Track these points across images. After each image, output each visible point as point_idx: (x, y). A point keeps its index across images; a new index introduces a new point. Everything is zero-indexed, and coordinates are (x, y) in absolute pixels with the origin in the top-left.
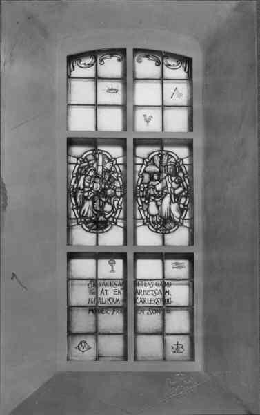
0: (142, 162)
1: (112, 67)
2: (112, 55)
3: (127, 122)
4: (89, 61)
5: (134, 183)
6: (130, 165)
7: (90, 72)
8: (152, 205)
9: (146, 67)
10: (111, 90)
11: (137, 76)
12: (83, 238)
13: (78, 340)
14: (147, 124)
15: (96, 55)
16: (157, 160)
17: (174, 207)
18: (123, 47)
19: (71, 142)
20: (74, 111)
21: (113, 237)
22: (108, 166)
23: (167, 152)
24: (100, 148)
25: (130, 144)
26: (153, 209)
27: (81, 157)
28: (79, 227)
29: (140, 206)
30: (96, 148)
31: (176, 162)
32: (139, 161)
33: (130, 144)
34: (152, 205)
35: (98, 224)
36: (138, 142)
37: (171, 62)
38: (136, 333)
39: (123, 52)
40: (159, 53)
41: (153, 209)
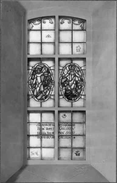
0: (62, 69)
1: (48, 24)
3: (57, 50)
5: (59, 78)
6: (57, 95)
9: (66, 25)
10: (48, 36)
11: (60, 41)
14: (65, 50)
15: (41, 19)
18: (54, 57)
19: (30, 60)
20: (31, 138)
21: (48, 104)
25: (57, 60)
27: (34, 67)
28: (33, 99)
29: (61, 89)
30: (41, 62)
33: (57, 60)
36: (60, 59)
38: (59, 42)
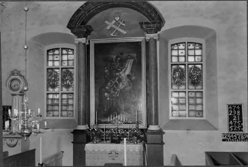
2: (57, 50)
4: (51, 51)
7: (52, 53)
8: (65, 82)
10: (182, 53)
12: (51, 90)
13: (49, 112)
16: (66, 73)
17: (70, 82)
22: (56, 74)
23: (68, 70)
24: (54, 70)
26: (65, 83)
31: (70, 73)
32: (173, 69)
34: (65, 82)
35: (54, 87)
37: (70, 50)
39: (185, 43)
40: (67, 48)
41: (65, 83)
